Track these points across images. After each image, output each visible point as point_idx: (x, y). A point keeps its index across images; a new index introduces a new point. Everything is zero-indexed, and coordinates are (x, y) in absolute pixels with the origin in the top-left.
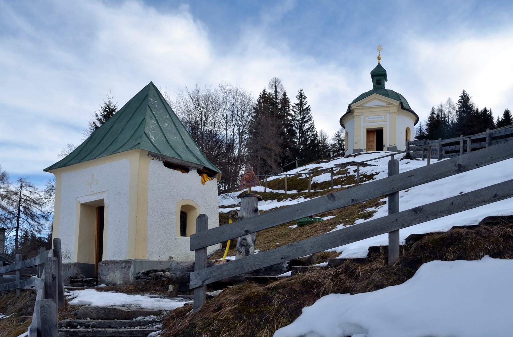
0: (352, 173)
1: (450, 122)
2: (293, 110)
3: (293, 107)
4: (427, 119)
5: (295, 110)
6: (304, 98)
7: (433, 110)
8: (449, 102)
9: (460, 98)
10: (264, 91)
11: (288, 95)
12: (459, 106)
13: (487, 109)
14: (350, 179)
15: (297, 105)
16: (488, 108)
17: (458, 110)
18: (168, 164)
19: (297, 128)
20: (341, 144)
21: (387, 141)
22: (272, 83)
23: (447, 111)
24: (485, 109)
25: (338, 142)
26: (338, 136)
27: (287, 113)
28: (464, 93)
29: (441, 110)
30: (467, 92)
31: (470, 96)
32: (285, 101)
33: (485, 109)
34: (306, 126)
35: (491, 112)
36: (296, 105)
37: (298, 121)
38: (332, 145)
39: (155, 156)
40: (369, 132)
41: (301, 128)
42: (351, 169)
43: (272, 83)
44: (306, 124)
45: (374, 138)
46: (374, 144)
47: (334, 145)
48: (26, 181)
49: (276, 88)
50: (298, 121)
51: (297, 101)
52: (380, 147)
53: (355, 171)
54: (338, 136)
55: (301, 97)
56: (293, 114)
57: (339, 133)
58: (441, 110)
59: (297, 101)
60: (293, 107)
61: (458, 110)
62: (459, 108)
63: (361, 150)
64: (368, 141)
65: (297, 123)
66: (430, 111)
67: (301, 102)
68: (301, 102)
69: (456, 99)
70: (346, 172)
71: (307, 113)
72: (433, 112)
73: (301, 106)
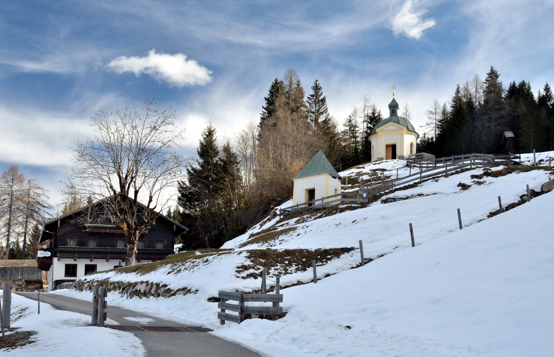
0: (380, 175)
1: (477, 104)
2: (307, 102)
3: (309, 98)
4: (451, 100)
5: (310, 101)
6: (320, 89)
7: (458, 89)
8: (476, 80)
9: (487, 76)
10: (276, 80)
11: (302, 85)
12: (487, 85)
13: (526, 82)
14: (379, 178)
15: (312, 96)
16: (526, 81)
17: (485, 89)
18: (333, 177)
19: (312, 121)
20: (353, 130)
21: (398, 153)
22: (287, 74)
23: (475, 90)
24: (524, 82)
25: (350, 128)
26: (350, 121)
27: (301, 103)
28: (492, 70)
29: (466, 89)
30: (496, 69)
31: (499, 73)
32: (300, 91)
33: (524, 82)
34: (321, 119)
35: (529, 87)
36: (311, 96)
37: (313, 113)
38: (342, 132)
39: (330, 175)
40: (387, 146)
41: (316, 120)
42: (379, 173)
43: (287, 74)
44: (321, 116)
45: (390, 150)
46: (390, 154)
47: (345, 132)
48: (35, 183)
49: (291, 78)
50: (313, 113)
51: (312, 92)
52: (394, 157)
53: (381, 174)
54: (350, 121)
55: (317, 88)
56: (308, 105)
57: (350, 117)
58: (466, 89)
59: (312, 92)
60: (309, 98)
61: (485, 89)
62: (487, 87)
63: (382, 159)
64: (387, 152)
65: (312, 115)
66: (455, 90)
67: (317, 93)
68: (317, 93)
69: (483, 77)
70: (376, 174)
71: (323, 104)
72: (458, 92)
73: (316, 97)
